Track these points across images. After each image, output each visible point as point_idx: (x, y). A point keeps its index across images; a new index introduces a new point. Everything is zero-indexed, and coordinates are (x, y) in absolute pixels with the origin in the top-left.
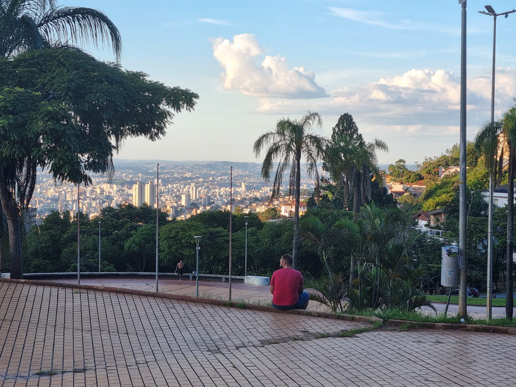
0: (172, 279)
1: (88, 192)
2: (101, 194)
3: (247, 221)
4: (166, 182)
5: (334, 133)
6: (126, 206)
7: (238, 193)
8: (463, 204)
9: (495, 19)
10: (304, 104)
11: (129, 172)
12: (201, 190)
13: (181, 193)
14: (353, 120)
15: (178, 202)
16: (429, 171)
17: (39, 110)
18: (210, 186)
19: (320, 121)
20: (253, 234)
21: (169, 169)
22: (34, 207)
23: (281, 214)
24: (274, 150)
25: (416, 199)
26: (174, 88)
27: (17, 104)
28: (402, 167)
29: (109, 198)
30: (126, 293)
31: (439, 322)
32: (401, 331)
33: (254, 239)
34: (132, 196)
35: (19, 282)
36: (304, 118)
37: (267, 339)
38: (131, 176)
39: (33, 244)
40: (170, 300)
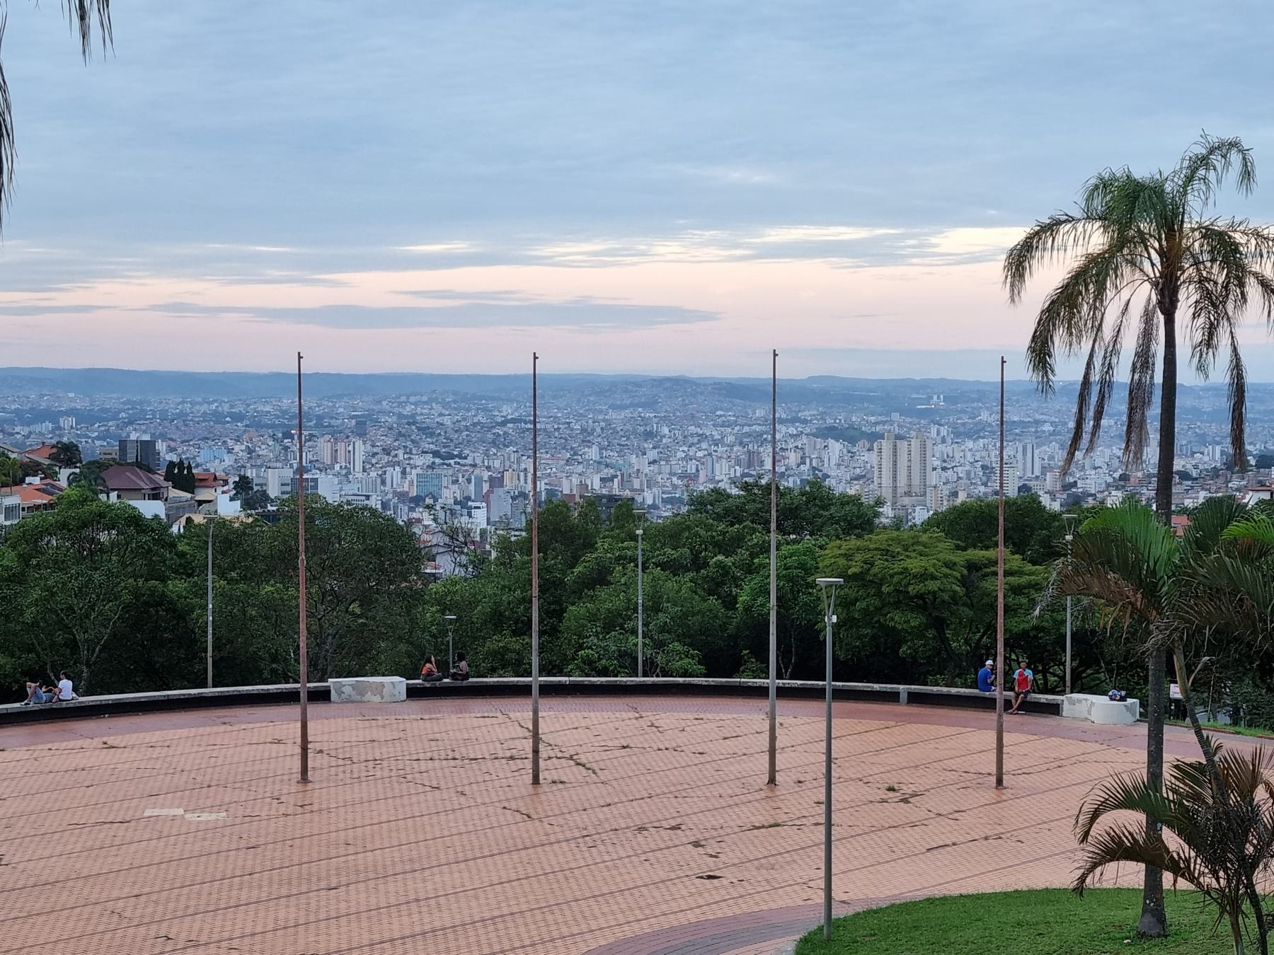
19: (1246, 166)
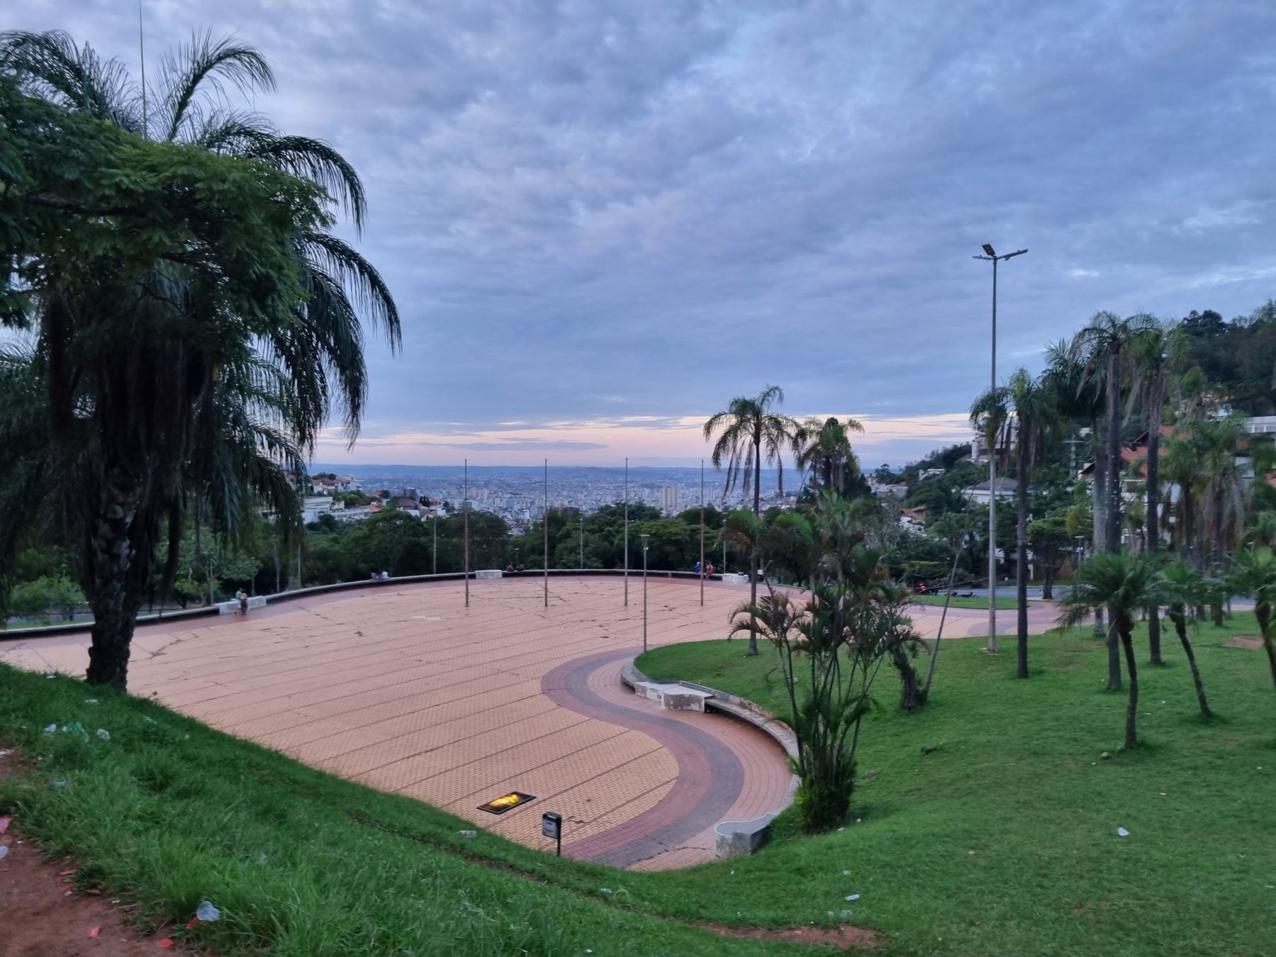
9: (995, 264)
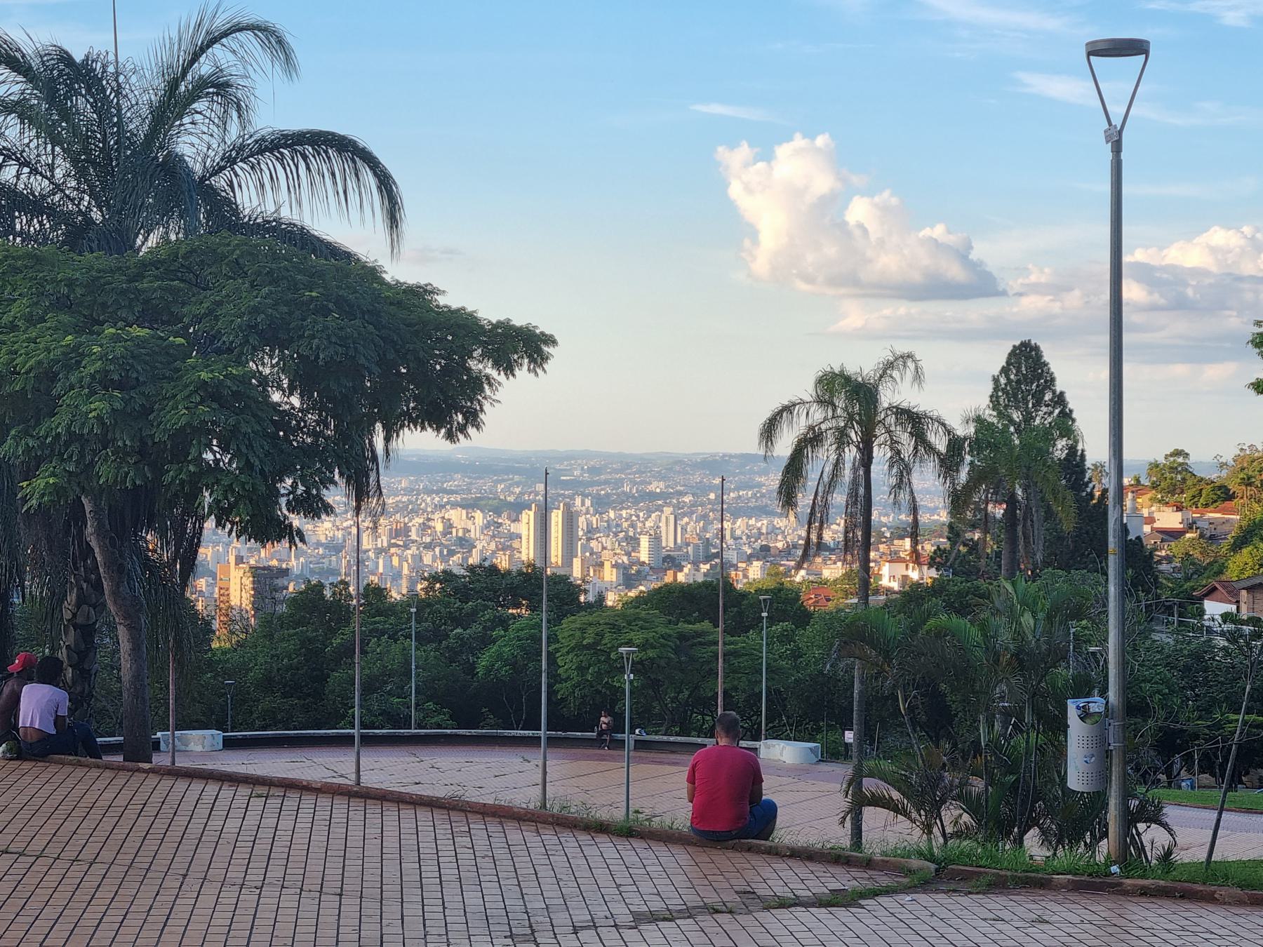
0: (585, 747)
1: (414, 529)
2: (445, 534)
3: (765, 608)
4: (601, 504)
5: (996, 389)
6: (485, 568)
7: (777, 531)
8: (1115, 601)
10: (948, 314)
11: (512, 479)
12: (687, 524)
13: (639, 530)
14: (1042, 356)
15: (633, 554)
16: (1249, 479)
17: (182, 376)
18: (711, 514)
20: (786, 638)
21: (610, 473)
22: (284, 566)
23: (880, 583)
24: (811, 439)
25: (1213, 548)
26: (499, 322)
27: (132, 366)
28: (1180, 469)
29: (465, 543)
30: (371, 798)
31: (1062, 874)
32: (970, 893)
33: (787, 649)
34: (521, 538)
35: (139, 770)
36: (881, 366)
37: (652, 910)
38: (517, 490)
39: (261, 660)
40: (466, 816)
